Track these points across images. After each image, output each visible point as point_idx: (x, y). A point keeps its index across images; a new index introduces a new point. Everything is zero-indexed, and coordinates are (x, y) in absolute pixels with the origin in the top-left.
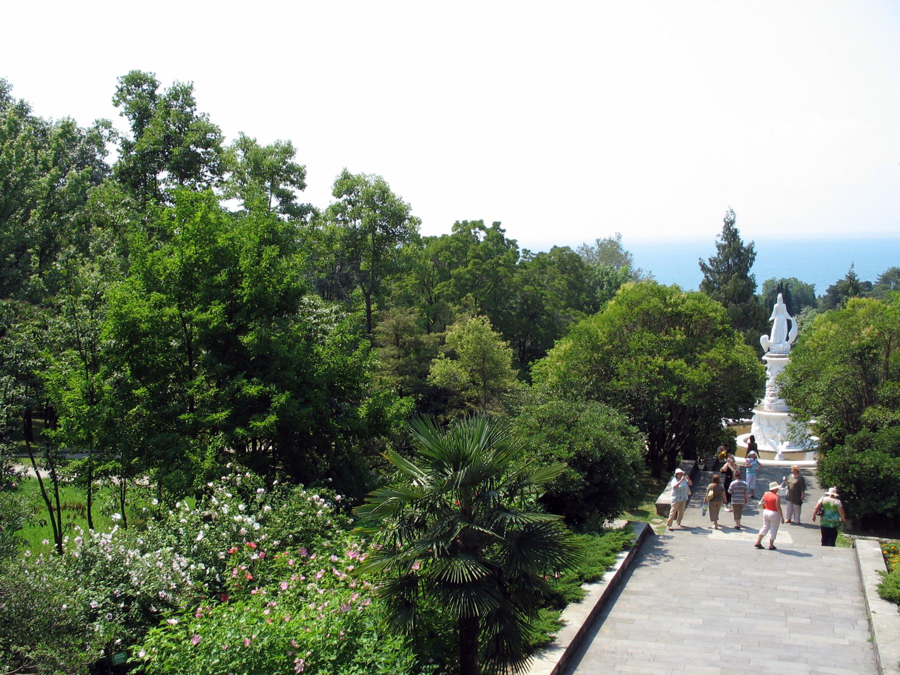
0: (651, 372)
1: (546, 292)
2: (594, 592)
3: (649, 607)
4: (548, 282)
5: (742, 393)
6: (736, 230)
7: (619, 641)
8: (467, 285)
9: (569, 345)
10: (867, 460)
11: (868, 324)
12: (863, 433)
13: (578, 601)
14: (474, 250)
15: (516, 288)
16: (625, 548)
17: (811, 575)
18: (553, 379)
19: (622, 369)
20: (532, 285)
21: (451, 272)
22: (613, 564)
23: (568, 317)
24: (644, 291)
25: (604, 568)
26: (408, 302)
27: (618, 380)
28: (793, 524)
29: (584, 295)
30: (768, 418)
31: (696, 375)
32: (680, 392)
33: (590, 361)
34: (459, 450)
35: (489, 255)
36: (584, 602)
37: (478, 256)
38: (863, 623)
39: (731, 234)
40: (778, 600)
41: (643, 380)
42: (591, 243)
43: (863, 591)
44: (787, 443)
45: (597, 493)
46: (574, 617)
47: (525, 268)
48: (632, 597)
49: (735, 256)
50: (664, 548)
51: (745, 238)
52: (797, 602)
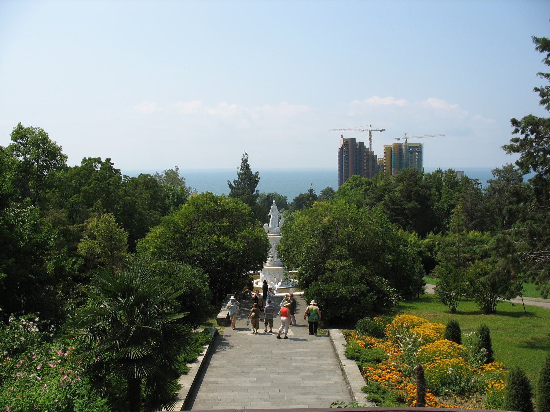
0: (210, 244)
1: (138, 200)
2: (194, 367)
3: (225, 374)
4: (139, 195)
5: (256, 255)
6: (248, 165)
7: (212, 394)
8: (90, 196)
9: (161, 229)
10: (330, 288)
11: (326, 216)
12: (327, 274)
13: (186, 373)
14: (95, 175)
15: (120, 198)
16: (207, 342)
17: (309, 350)
18: (153, 249)
19: (193, 242)
20: (130, 196)
21: (81, 189)
22: (202, 352)
23: (151, 215)
24: (205, 198)
25: (197, 354)
26: (60, 206)
27: (191, 249)
28: (293, 326)
29: (159, 203)
30: (269, 270)
31: (237, 245)
32: (227, 256)
33: (174, 239)
34: (128, 285)
35: (104, 178)
36: (190, 374)
37: (97, 179)
38: (339, 372)
39: (245, 166)
40: (294, 364)
41: (206, 248)
42: (161, 172)
43: (337, 356)
44: (280, 283)
45: (198, 308)
46: (185, 382)
47: (125, 186)
48: (214, 369)
49: (247, 179)
50: (227, 342)
51: (254, 169)
52: (304, 364)
